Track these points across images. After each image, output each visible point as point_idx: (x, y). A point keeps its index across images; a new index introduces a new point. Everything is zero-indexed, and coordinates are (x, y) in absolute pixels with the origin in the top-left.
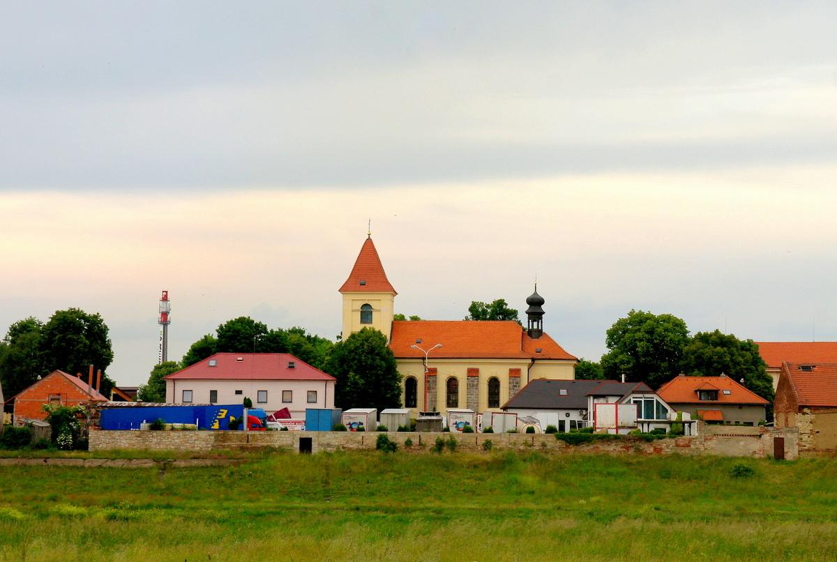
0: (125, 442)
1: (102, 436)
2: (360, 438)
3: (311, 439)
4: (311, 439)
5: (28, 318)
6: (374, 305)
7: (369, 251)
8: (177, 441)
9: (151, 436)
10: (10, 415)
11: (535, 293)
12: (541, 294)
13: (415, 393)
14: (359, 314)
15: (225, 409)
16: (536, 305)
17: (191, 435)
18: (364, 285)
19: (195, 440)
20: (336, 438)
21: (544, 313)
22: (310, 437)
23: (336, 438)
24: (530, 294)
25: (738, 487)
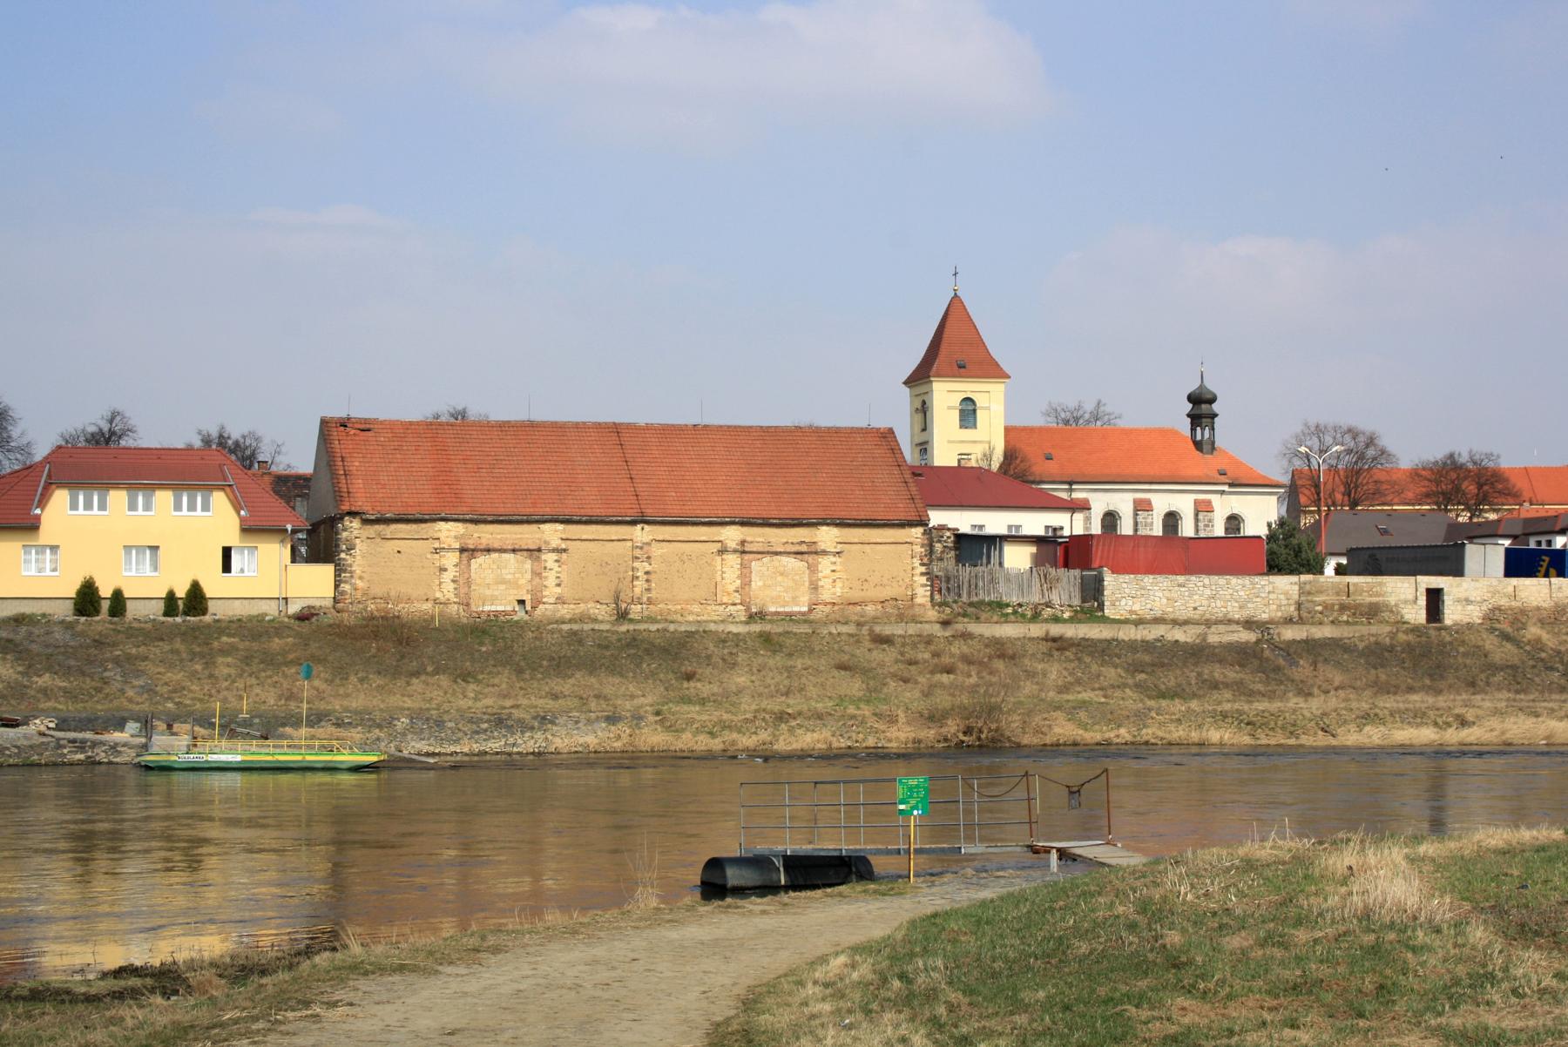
0: (1161, 595)
1: (1125, 585)
2: (1511, 589)
3: (1442, 589)
4: (1442, 589)
5: (1487, 450)
6: (980, 400)
7: (954, 314)
8: (1242, 593)
9: (1201, 584)
10: (327, 570)
11: (1202, 386)
12: (1211, 385)
13: (593, 528)
14: (957, 413)
15: (1546, 555)
16: (1201, 407)
17: (1263, 583)
18: (964, 367)
19: (1269, 592)
20: (1477, 589)
21: (1216, 415)
22: (1440, 587)
23: (1477, 589)
24: (1192, 386)
25: (796, 679)
